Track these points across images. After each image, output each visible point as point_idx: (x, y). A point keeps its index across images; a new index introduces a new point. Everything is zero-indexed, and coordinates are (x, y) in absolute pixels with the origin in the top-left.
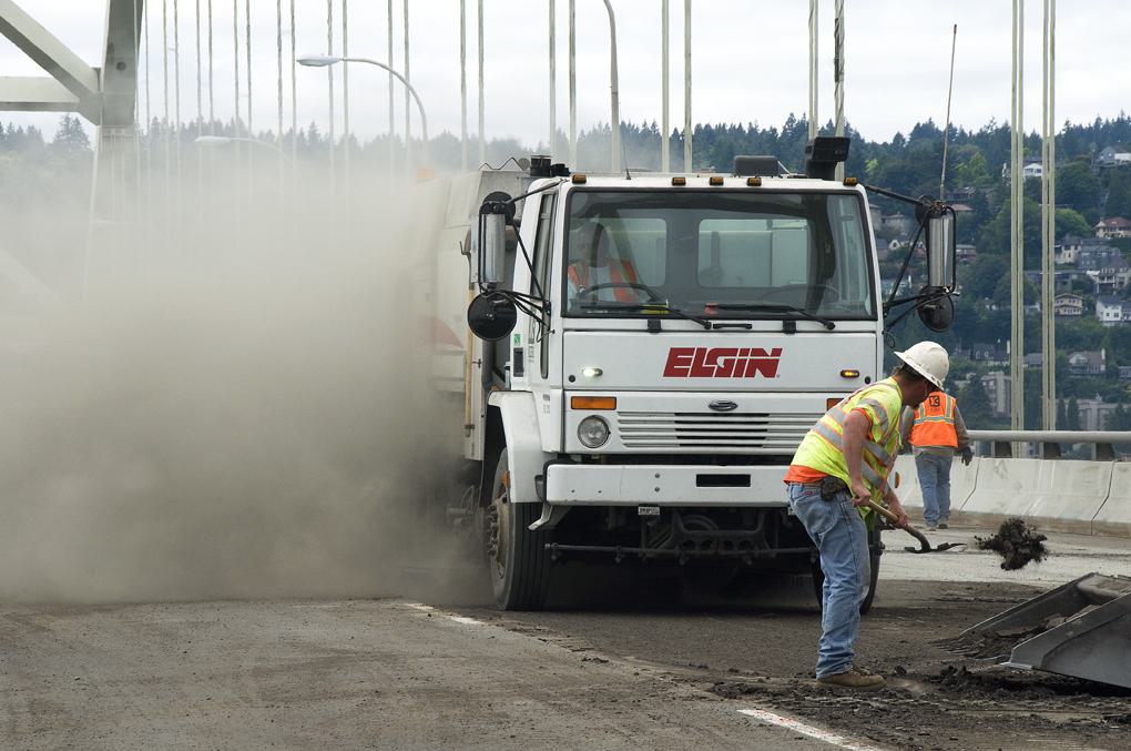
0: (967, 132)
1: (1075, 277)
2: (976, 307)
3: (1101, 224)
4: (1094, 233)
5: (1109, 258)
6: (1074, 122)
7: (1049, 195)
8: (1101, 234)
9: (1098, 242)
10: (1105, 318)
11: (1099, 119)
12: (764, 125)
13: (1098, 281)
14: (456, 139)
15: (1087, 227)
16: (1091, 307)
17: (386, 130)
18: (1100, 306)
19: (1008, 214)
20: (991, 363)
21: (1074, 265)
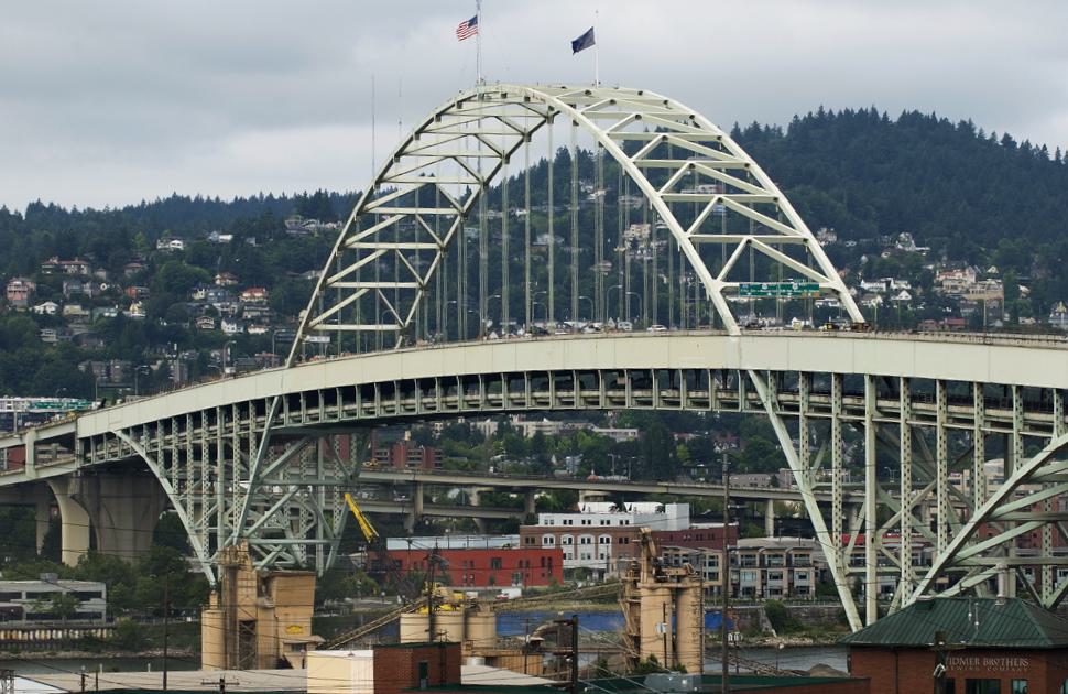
0: (205, 198)
1: (207, 307)
2: (155, 323)
3: (218, 276)
4: (214, 281)
5: (224, 296)
6: (179, 194)
7: (655, 264)
8: (218, 282)
9: (217, 286)
10: (226, 330)
11: (144, 202)
12: (97, 209)
13: (220, 309)
14: (953, 126)
15: (210, 278)
16: (218, 325)
17: (168, 673)
18: (224, 324)
19: (717, 313)
20: (737, 553)
21: (205, 299)
